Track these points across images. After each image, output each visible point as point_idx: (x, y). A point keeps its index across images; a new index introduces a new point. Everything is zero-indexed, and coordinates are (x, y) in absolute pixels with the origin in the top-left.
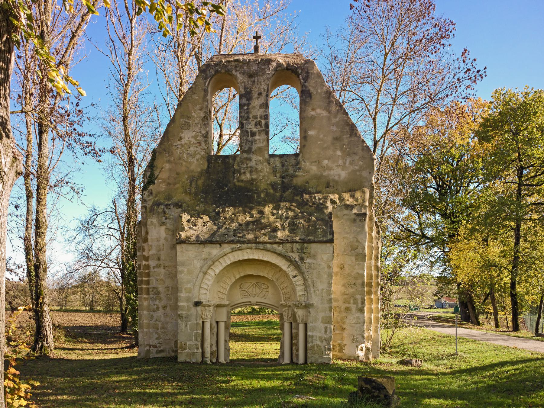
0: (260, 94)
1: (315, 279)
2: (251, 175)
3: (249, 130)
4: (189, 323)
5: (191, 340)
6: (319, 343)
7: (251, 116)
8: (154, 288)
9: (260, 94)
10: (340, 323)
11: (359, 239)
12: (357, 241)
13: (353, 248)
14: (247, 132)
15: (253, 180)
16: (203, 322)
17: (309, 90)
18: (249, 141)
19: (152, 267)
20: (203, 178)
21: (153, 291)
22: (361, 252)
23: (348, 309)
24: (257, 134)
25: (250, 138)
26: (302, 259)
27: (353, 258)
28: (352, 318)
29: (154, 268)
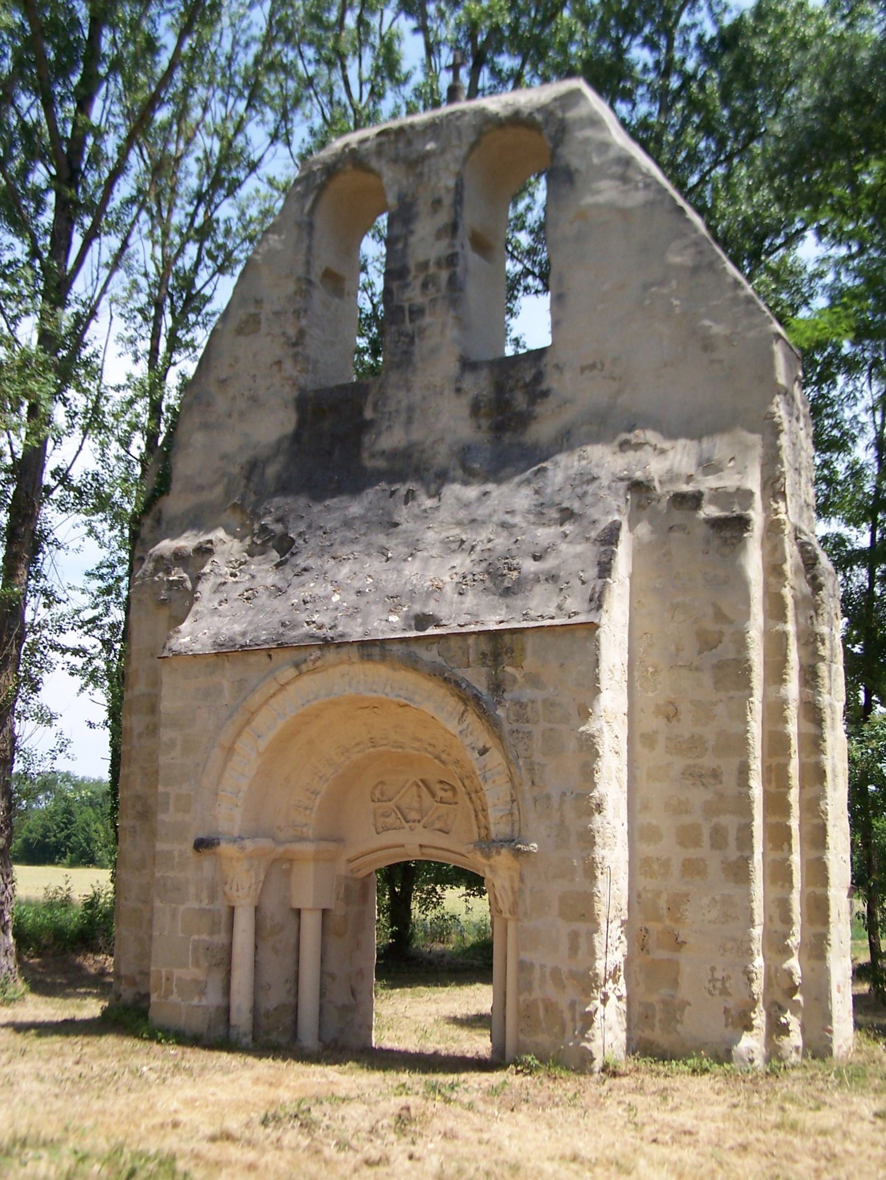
0: (437, 203)
1: (537, 758)
2: (407, 433)
3: (406, 305)
4: (182, 908)
5: (184, 965)
6: (550, 990)
7: (412, 265)
8: (139, 797)
9: (437, 203)
10: (668, 922)
11: (726, 610)
12: (720, 616)
13: (707, 643)
14: (401, 309)
15: (411, 446)
16: (232, 910)
17: (568, 166)
18: (407, 335)
19: (135, 733)
20: (281, 459)
21: (134, 806)
22: (731, 656)
23: (693, 868)
24: (427, 311)
25: (408, 326)
26: (497, 687)
27: (707, 679)
28: (706, 901)
29: (140, 735)
